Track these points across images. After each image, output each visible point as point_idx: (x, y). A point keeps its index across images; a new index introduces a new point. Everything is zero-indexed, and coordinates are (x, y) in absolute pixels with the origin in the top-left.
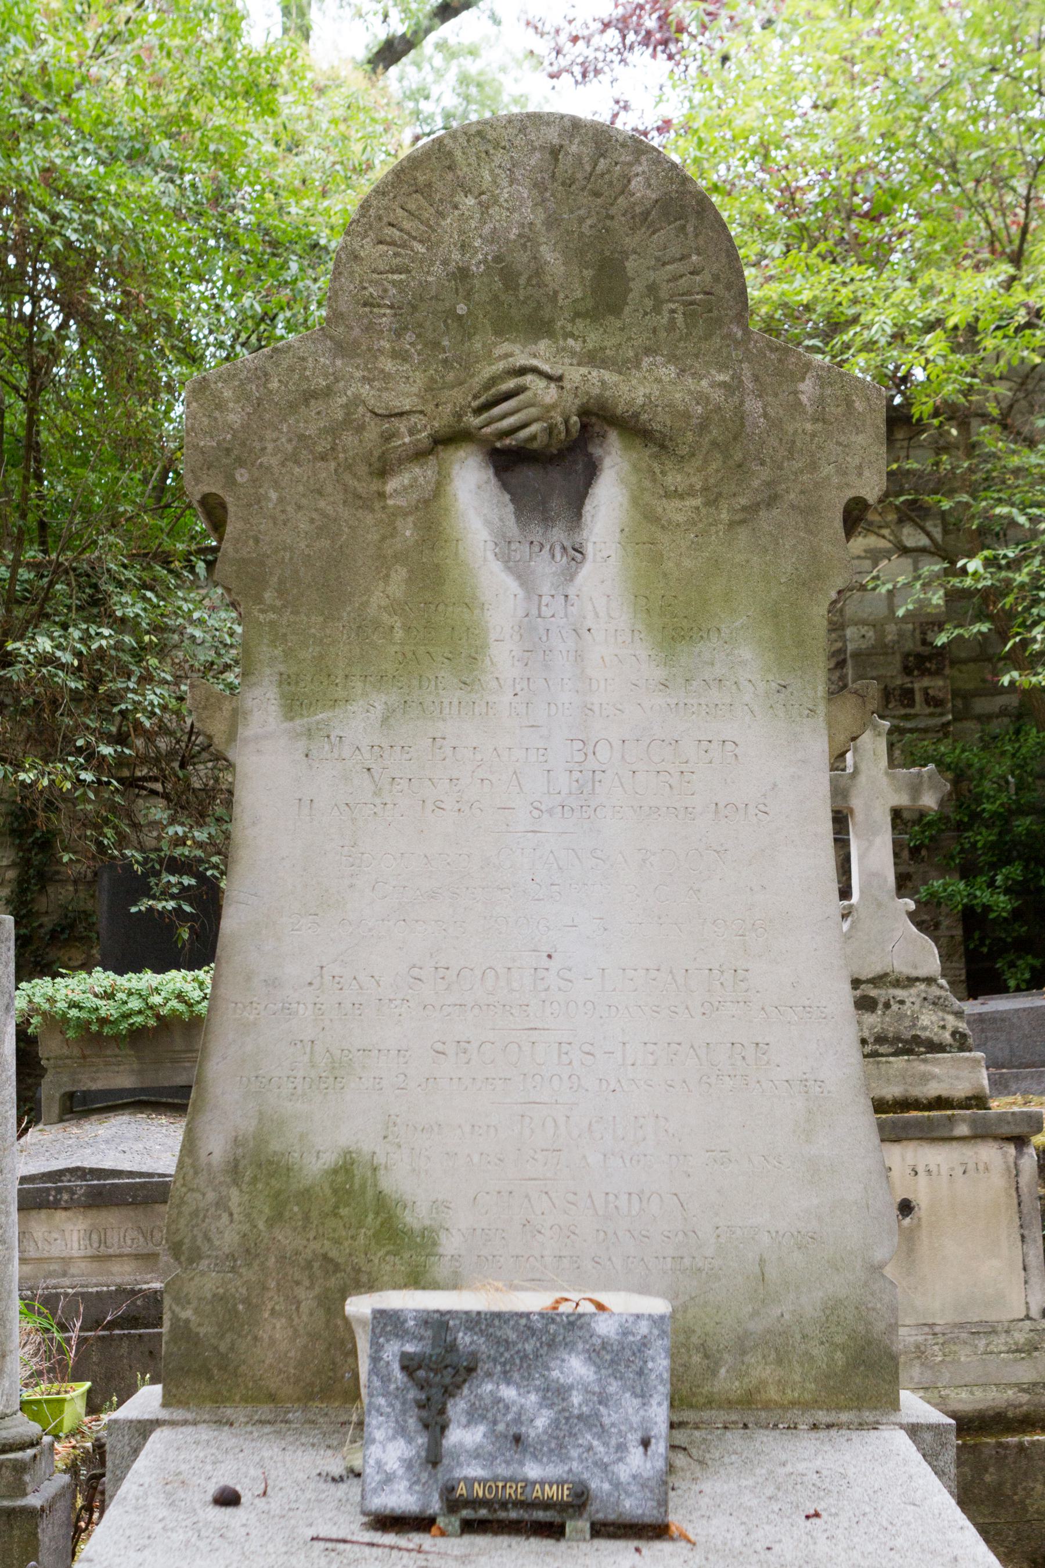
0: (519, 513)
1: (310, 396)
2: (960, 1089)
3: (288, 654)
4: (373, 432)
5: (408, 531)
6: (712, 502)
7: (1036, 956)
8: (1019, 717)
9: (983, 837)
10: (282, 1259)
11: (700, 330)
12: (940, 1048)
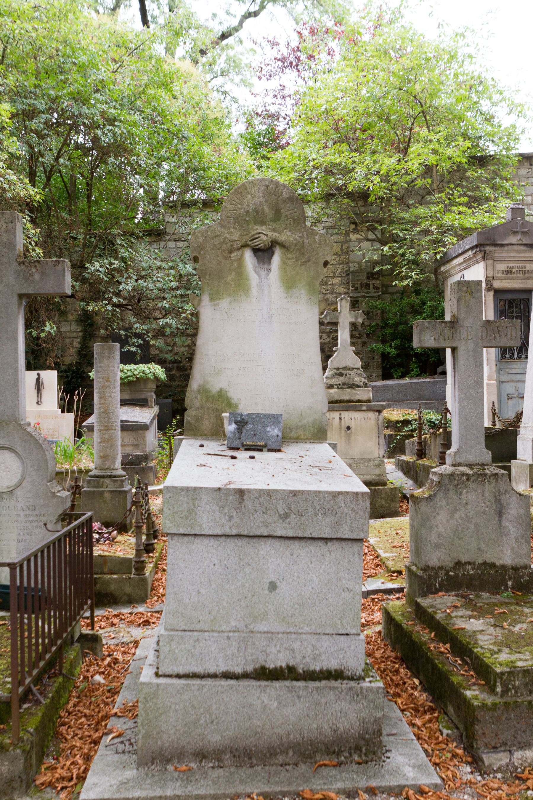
0: (258, 262)
1: (216, 236)
2: (365, 398)
3: (211, 289)
4: (229, 245)
5: (236, 264)
6: (297, 261)
7: (403, 368)
8: (403, 294)
9: (389, 331)
10: (208, 409)
11: (296, 225)
12: (358, 386)
